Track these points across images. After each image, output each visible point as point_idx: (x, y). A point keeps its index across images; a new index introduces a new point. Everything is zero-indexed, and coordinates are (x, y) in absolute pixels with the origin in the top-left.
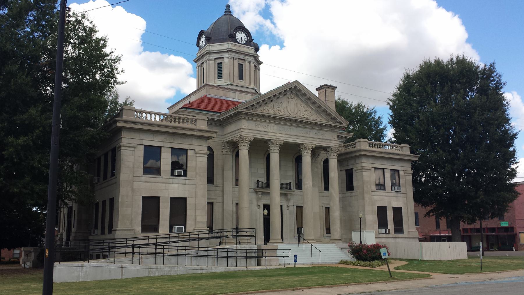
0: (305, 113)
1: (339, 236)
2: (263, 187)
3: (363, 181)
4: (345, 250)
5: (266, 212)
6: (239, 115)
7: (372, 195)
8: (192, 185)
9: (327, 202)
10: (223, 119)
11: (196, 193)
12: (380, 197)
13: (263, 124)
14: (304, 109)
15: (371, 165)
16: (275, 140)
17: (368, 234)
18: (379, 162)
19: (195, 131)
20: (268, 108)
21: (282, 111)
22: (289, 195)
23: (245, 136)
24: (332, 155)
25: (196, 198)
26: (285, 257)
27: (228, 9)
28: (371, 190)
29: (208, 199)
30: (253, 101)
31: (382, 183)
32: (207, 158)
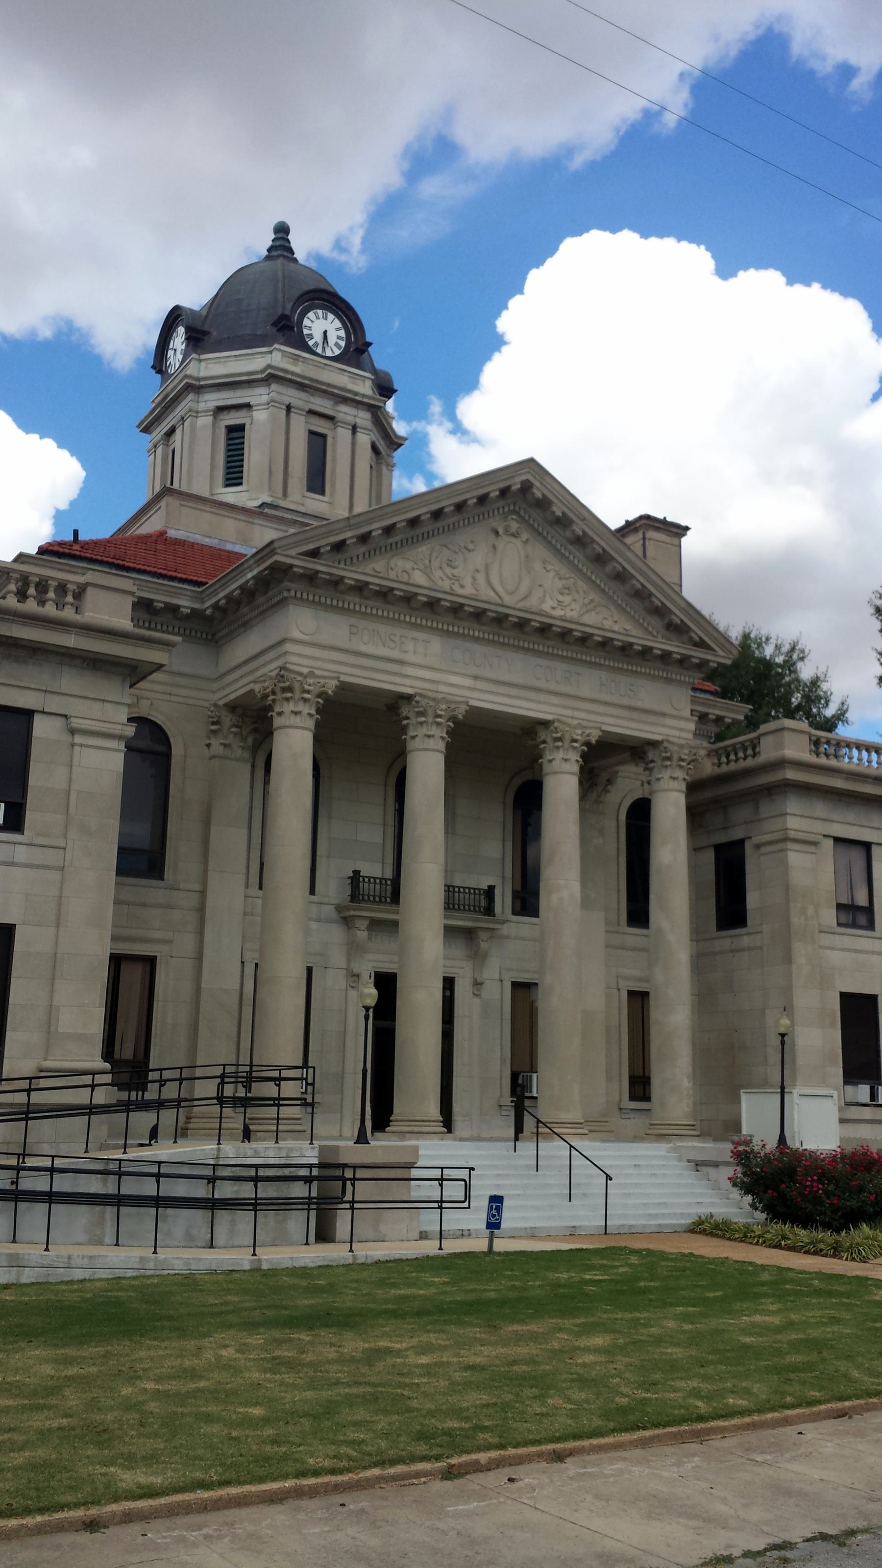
0: (561, 598)
1: (686, 1109)
2: (381, 900)
3: (787, 888)
4: (711, 1171)
5: (370, 995)
6: (280, 581)
7: (821, 947)
8: (48, 867)
9: (636, 973)
10: (215, 606)
11: (60, 905)
12: (854, 955)
13: (385, 629)
14: (559, 584)
15: (820, 828)
16: (434, 700)
17: (806, 1103)
18: (851, 816)
19: (69, 632)
20: (408, 565)
21: (468, 581)
22: (483, 935)
23: (301, 674)
24: (666, 774)
25: (58, 926)
26: (444, 1205)
27: (282, 239)
28: (820, 925)
29: (115, 938)
30: (341, 525)
31: (862, 899)
32: (122, 756)
